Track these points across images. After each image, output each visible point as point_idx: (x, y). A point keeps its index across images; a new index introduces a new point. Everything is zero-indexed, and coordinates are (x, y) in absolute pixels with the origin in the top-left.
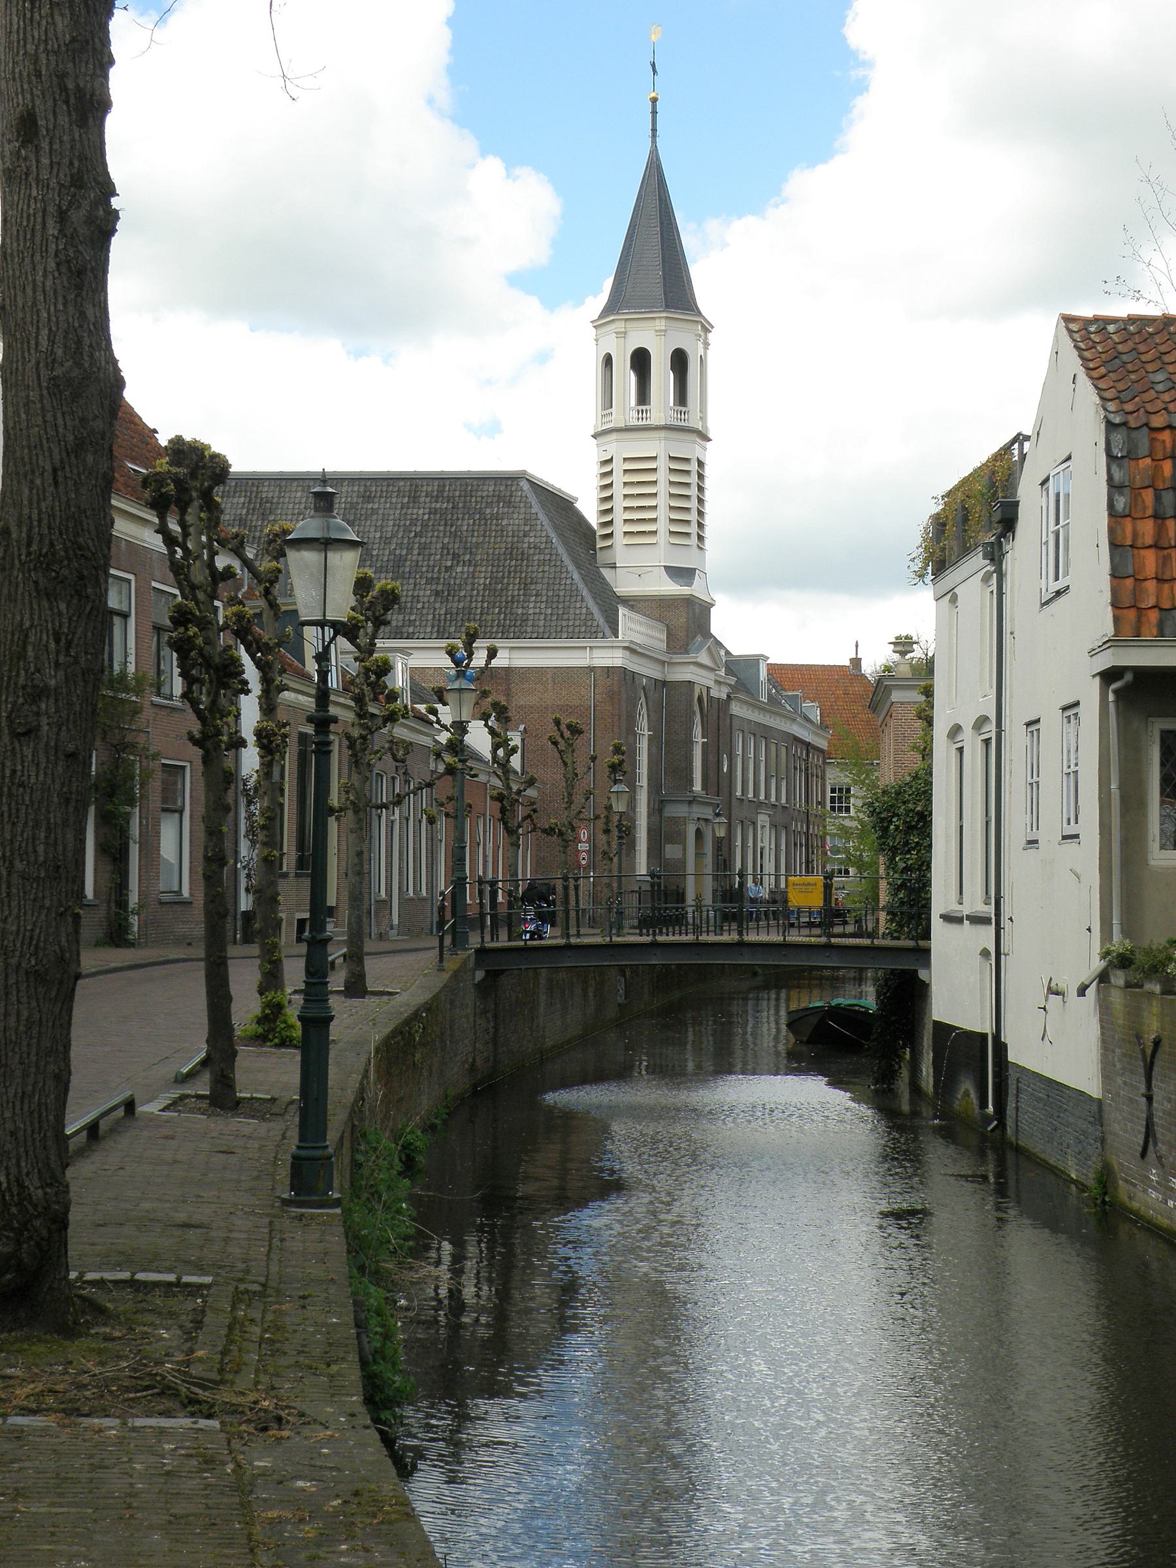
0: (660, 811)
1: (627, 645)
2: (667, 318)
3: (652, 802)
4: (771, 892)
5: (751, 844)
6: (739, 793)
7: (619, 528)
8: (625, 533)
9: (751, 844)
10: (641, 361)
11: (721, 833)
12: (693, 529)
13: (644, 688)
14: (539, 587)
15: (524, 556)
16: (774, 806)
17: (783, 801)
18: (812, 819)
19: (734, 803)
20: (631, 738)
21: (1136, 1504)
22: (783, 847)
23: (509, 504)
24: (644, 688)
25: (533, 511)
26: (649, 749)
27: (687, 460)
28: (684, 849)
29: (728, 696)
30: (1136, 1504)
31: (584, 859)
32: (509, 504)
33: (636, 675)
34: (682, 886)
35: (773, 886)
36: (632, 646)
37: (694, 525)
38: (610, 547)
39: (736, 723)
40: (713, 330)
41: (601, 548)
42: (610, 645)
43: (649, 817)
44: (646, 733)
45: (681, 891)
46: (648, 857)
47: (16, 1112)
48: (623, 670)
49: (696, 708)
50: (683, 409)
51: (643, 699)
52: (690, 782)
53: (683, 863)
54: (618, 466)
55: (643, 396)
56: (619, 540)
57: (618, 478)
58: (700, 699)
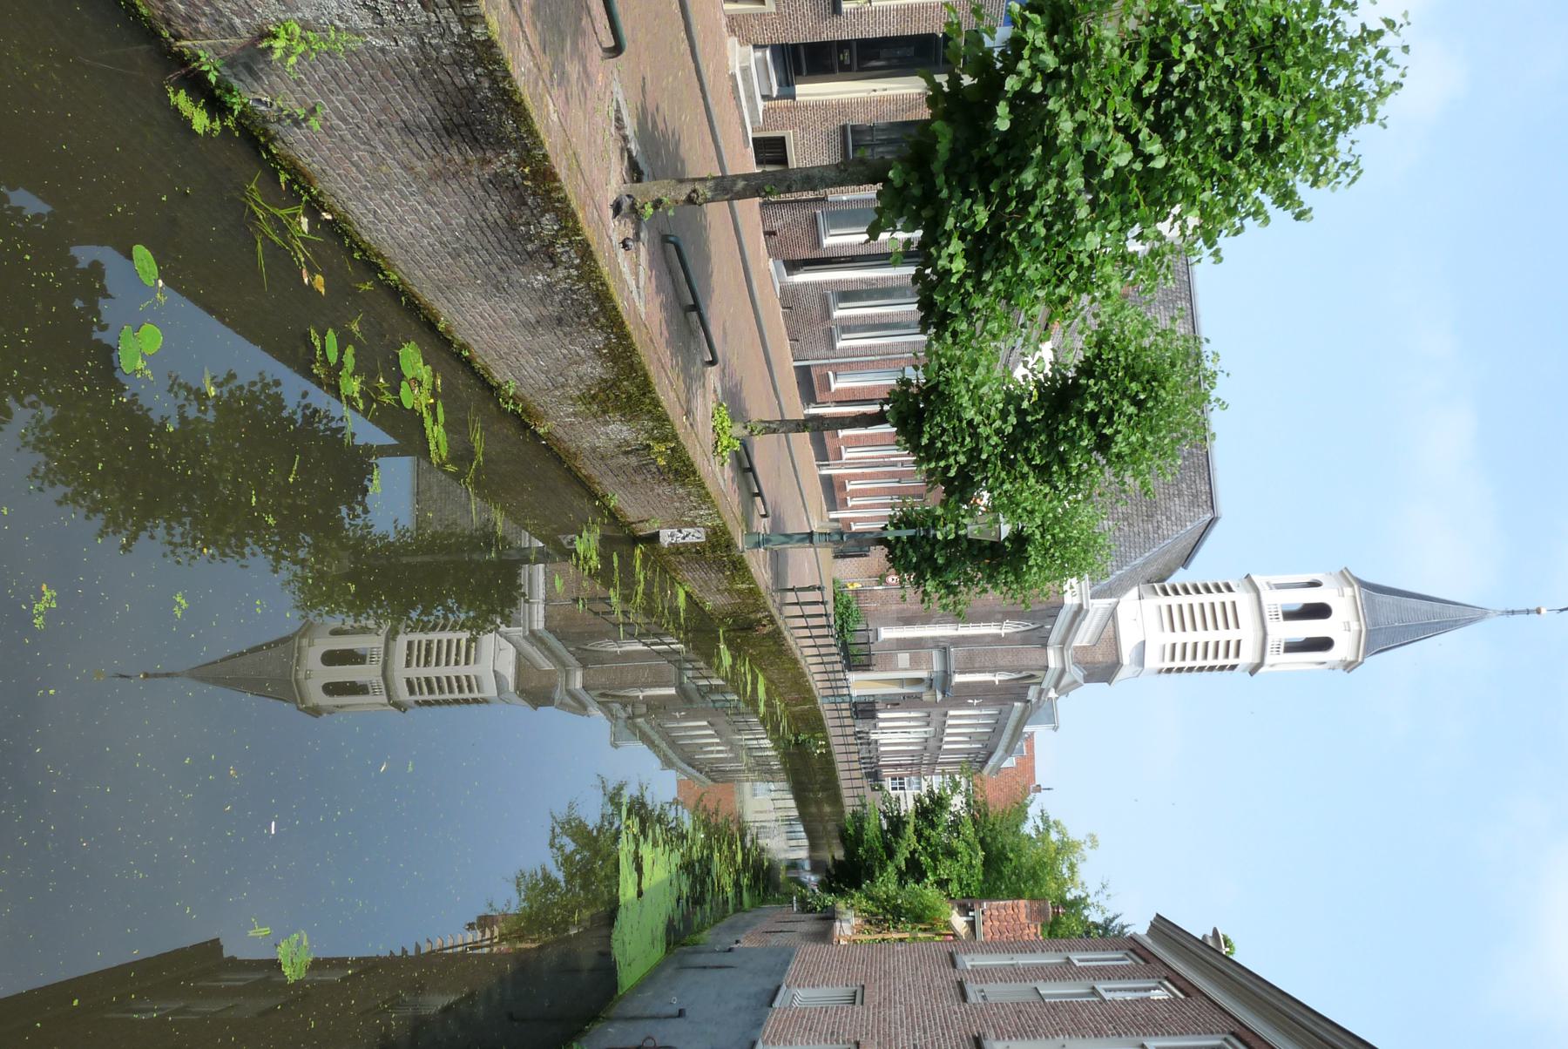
0: (937, 647)
1: (1085, 607)
2: (1361, 631)
4: (876, 741)
5: (912, 724)
6: (951, 713)
7: (1174, 600)
8: (1160, 607)
9: (912, 724)
10: (1320, 611)
11: (926, 697)
12: (1178, 663)
13: (1042, 627)
14: (1126, 529)
15: (1150, 516)
16: (942, 740)
17: (945, 747)
18: (931, 767)
19: (944, 710)
20: (1000, 616)
21: (266, 407)
22: (911, 748)
23: (1192, 503)
24: (1042, 627)
25: (1188, 524)
26: (988, 635)
27: (1237, 655)
28: (906, 669)
29: (1029, 701)
30: (266, 407)
32: (1192, 503)
33: (1053, 619)
34: (875, 668)
35: (881, 742)
36: (1083, 612)
37: (1181, 664)
38: (1156, 593)
39: (1005, 708)
40: (1345, 673)
41: (1154, 587)
42: (1084, 592)
46: (898, 639)
47: (484, 223)
48: (1061, 606)
50: (1282, 649)
51: (1032, 626)
52: (962, 672)
53: (896, 669)
54: (1227, 597)
55: (1290, 615)
56: (1164, 601)
57: (1216, 598)
58: (1032, 676)
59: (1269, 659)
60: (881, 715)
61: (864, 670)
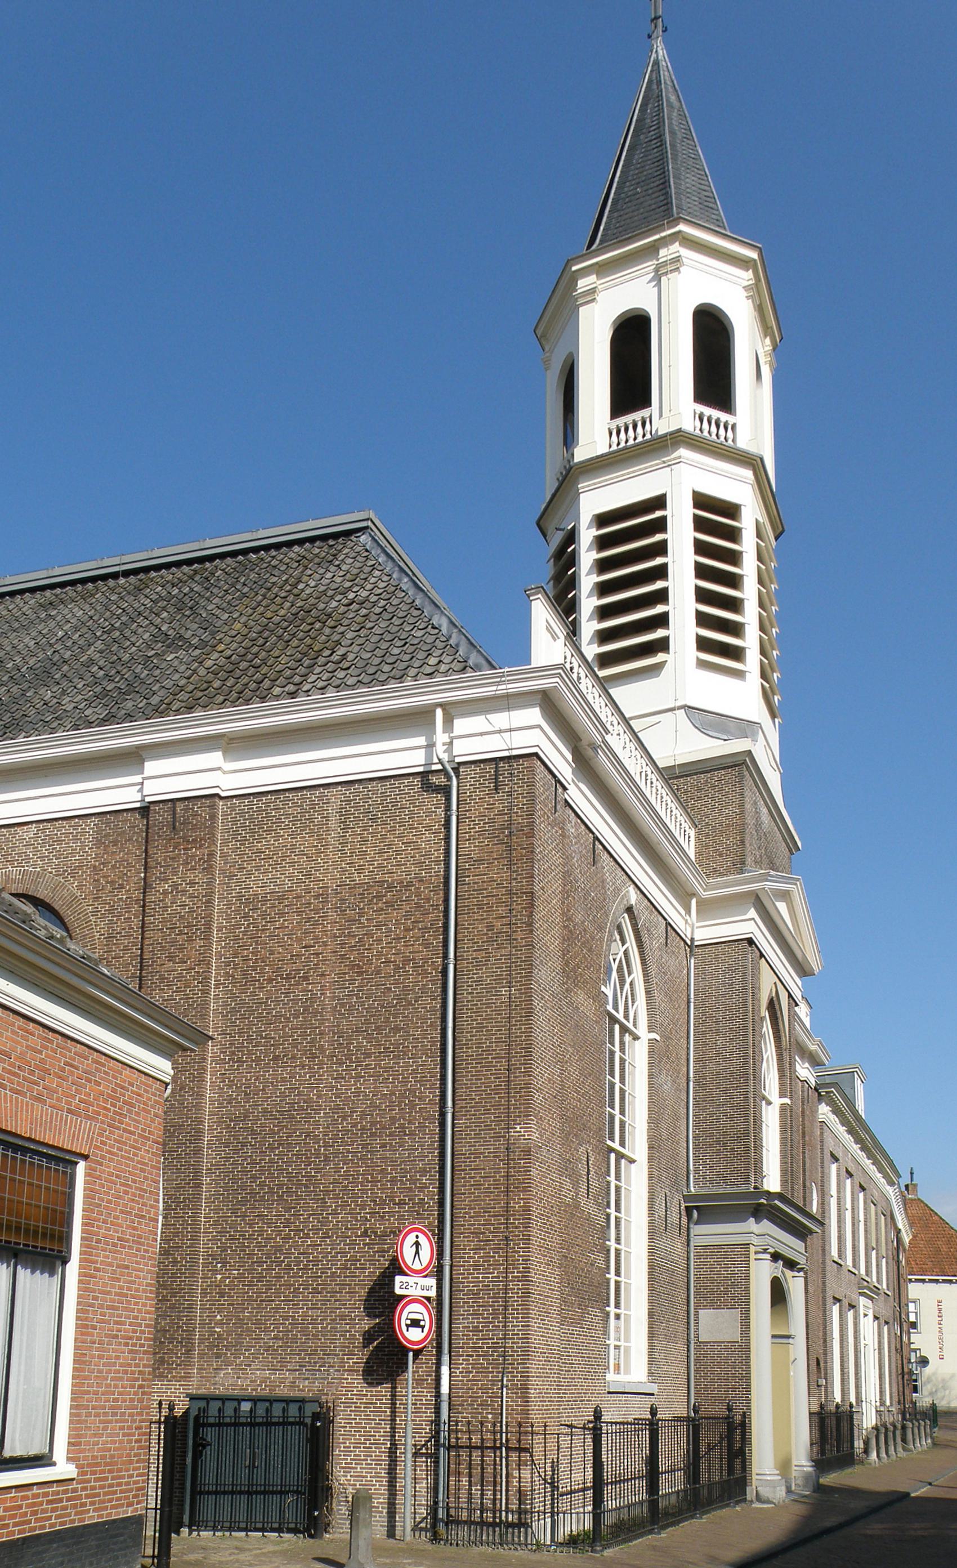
3: (660, 1201)
19: (831, 1268)
31: (415, 1323)
43: (653, 1234)
44: (642, 1029)
45: (738, 1418)
49: (767, 1028)
53: (743, 1350)
59: (744, 442)
60: (838, 1398)
61: (745, 1439)
